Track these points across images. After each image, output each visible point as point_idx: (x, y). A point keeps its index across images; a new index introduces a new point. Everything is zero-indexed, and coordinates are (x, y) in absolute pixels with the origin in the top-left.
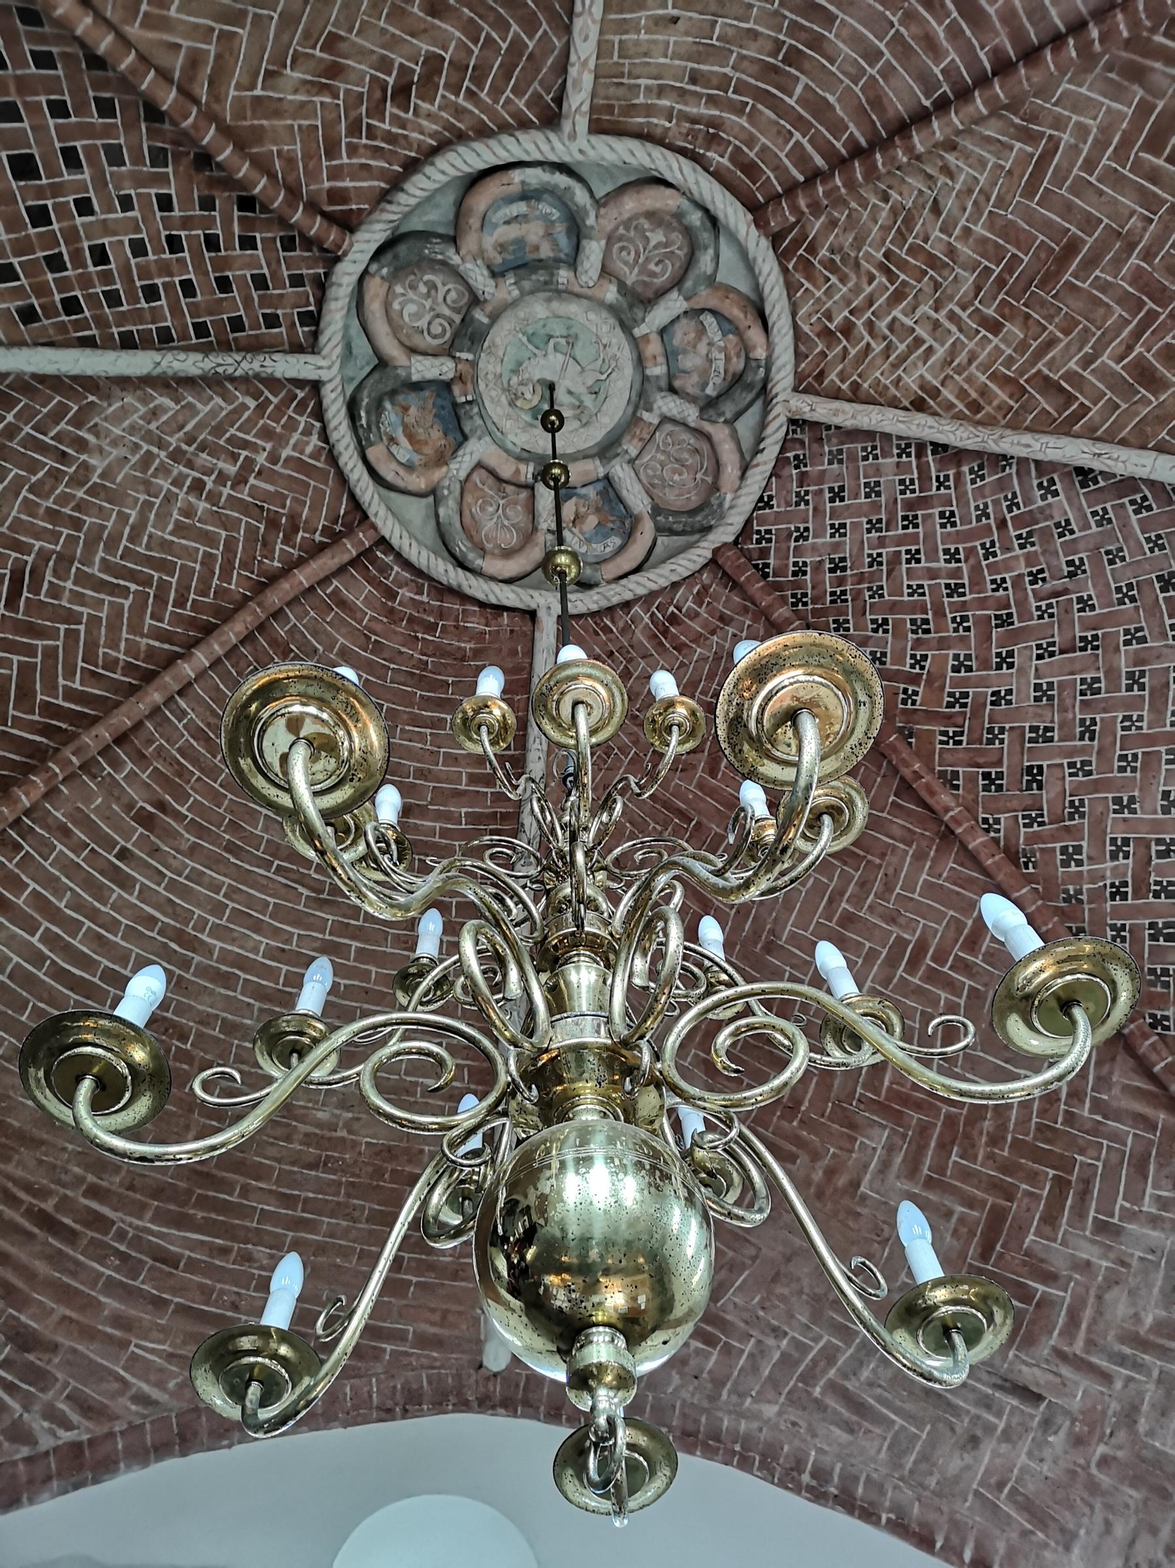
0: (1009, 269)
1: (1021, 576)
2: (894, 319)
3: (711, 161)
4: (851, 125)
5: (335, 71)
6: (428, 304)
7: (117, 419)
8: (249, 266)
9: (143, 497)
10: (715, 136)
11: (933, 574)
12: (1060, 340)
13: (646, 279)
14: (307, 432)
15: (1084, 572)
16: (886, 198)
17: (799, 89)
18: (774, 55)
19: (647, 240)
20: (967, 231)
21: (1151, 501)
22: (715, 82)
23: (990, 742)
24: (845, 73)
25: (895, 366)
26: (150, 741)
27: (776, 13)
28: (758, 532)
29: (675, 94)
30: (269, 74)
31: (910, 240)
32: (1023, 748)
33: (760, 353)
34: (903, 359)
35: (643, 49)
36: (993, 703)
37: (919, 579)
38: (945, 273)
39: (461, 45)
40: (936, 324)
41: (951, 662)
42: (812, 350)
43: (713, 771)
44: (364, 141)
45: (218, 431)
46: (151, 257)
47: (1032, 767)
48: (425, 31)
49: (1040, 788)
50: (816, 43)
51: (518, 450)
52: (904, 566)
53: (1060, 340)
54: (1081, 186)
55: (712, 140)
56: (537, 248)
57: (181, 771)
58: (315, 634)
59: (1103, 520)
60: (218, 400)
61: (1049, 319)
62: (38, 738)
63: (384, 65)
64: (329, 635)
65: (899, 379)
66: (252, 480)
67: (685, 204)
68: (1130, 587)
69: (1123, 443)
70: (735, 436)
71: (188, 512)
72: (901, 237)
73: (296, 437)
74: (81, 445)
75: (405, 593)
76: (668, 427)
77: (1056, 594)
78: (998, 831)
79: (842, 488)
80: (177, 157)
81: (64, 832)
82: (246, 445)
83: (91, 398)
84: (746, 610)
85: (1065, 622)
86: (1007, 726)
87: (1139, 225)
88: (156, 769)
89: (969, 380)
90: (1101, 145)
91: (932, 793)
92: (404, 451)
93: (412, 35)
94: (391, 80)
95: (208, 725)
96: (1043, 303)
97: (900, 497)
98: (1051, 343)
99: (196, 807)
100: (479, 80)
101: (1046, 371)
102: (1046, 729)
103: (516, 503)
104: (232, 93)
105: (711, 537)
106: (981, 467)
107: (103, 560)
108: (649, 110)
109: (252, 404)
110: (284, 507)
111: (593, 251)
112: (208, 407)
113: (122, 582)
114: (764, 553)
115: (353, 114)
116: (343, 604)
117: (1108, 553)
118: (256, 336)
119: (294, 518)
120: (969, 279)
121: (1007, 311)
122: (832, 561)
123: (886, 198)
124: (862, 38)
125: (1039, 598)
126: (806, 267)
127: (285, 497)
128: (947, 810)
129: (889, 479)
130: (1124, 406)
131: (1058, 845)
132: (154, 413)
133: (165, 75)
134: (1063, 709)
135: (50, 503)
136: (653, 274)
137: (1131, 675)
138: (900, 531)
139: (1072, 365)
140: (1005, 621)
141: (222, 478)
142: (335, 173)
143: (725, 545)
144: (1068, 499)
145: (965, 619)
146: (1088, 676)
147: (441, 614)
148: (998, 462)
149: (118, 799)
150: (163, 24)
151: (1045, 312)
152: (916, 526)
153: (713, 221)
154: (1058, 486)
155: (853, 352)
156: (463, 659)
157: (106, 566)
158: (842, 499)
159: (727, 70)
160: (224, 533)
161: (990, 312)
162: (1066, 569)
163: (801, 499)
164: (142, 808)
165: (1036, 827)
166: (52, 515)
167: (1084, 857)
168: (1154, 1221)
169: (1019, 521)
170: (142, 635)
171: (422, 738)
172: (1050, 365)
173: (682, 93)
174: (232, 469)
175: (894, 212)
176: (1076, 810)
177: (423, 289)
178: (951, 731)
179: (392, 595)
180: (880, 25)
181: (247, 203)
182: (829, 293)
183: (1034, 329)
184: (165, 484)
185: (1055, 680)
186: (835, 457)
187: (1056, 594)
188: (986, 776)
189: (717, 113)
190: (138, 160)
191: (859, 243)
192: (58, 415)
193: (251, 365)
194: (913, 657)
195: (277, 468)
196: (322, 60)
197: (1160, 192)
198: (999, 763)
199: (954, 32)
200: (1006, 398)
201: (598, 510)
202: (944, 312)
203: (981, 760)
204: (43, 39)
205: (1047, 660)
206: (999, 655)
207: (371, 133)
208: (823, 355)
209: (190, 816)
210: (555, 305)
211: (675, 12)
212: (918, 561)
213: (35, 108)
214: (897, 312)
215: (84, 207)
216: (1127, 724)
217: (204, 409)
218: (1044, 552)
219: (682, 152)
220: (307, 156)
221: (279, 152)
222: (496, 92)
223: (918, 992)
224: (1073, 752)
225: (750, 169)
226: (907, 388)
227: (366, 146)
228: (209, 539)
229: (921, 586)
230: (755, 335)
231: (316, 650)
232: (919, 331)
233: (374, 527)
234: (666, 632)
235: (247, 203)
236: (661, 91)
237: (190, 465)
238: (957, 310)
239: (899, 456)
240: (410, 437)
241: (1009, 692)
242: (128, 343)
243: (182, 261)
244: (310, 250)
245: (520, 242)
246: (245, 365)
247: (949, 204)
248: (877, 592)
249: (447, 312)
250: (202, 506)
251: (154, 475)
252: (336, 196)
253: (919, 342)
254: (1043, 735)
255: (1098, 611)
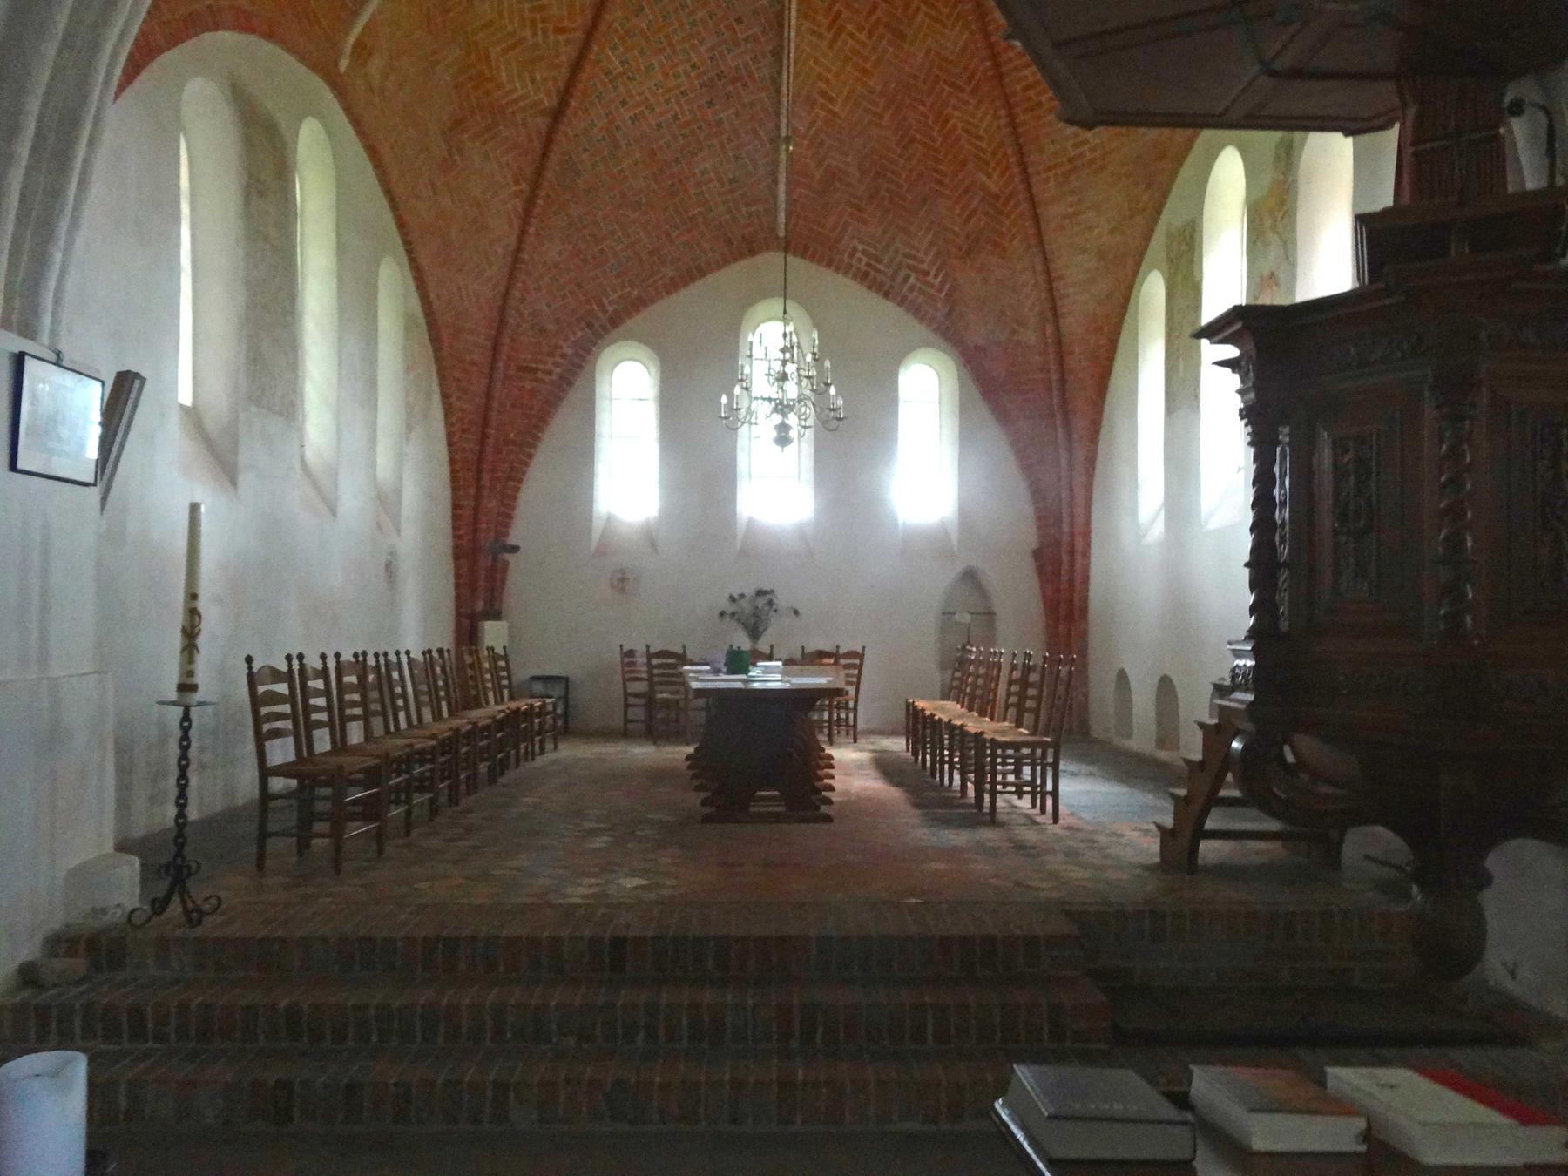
168: (501, 166)
223: (523, 20)
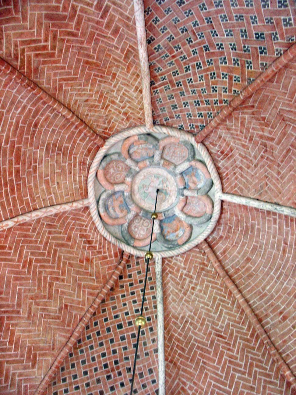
0: (97, 76)
1: (190, 46)
2: (120, 102)
3: (89, 162)
4: (71, 130)
5: (88, 260)
6: (140, 228)
7: (175, 309)
8: (136, 276)
9: (197, 302)
10: (83, 163)
11: (195, 74)
12: (113, 57)
13: (124, 169)
14: (177, 260)
15: (184, 27)
16: (87, 115)
17: (67, 145)
18: (60, 154)
19: (113, 173)
20: (90, 90)
21: (154, 18)
22: (70, 167)
23: (249, 51)
24: (60, 136)
25: (132, 99)
26: (262, 312)
27: (51, 157)
28: (191, 128)
29: (75, 177)
30: (90, 276)
31: (97, 104)
32: (250, 40)
33: (136, 138)
34: (130, 98)
35: (66, 189)
36: (235, 50)
37: (197, 78)
38: (103, 92)
39: (76, 230)
40: (118, 90)
41: (223, 65)
42: (133, 122)
43: (272, 139)
44: (102, 249)
45: (178, 284)
46: (136, 299)
47: (256, 37)
48: (75, 240)
49: (263, 34)
50: (54, 145)
51: (177, 199)
52: (194, 83)
53: (113, 57)
54: (70, 67)
55: (84, 163)
56: (121, 202)
57: (272, 305)
58: (233, 261)
59: (165, 29)
60: (169, 284)
61: (107, 61)
62: (259, 342)
63: (84, 248)
64: (234, 257)
65: (135, 97)
66: (191, 274)
67: (101, 168)
68: (186, 13)
69: (136, 34)
70: (163, 139)
71: (201, 291)
72: (97, 106)
73: (178, 263)
74: (183, 318)
75: (221, 233)
76: (164, 156)
77: (194, 34)
78: (281, 50)
79: (172, 106)
80: (112, 295)
81: (285, 342)
82: (181, 276)
83: (170, 316)
84: (215, 132)
85: (203, 28)
86: (243, 45)
87: (74, 48)
88: (271, 312)
89: (131, 79)
90: (57, 68)
91: (267, 76)
92: (180, 233)
93: (76, 242)
94: (87, 245)
95: (259, 295)
96: (104, 64)
97: (171, 89)
98: (114, 59)
99: (283, 303)
100: (83, 225)
101: (123, 59)
102: (242, 31)
103: (192, 200)
104: (96, 284)
105: (194, 144)
106: (156, 70)
107: (214, 313)
108: (80, 183)
109: (170, 275)
110: (198, 266)
111: (117, 188)
112: (171, 287)
113: (219, 310)
114: (197, 127)
115: (96, 253)
116: (224, 252)
117: (176, 23)
118: (152, 274)
119: (200, 264)
120: (103, 85)
121: (109, 73)
122: (196, 105)
123: (87, 115)
124: (50, 135)
125: (197, 39)
126: (111, 129)
127: (195, 266)
128: (273, 71)
129: (166, 94)
130: (126, 36)
131: (284, 28)
132: (174, 300)
133: (94, 301)
134: (233, 26)
135: (199, 325)
136: (122, 168)
137: (217, 6)
138: (183, 86)
139: (119, 52)
140: (207, 48)
141: (191, 282)
142: (111, 256)
143: (195, 139)
144: (160, 41)
145: (208, 62)
146: (220, 19)
147: (226, 224)
148: (152, 66)
149: (277, 325)
150: (83, 301)
151: (106, 63)
152: (180, 82)
153: (105, 157)
154: (156, 46)
155: (131, 111)
156: (238, 220)
157: (215, 313)
158: (176, 105)
159: (67, 165)
160: (205, 283)
161: (110, 77)
162: (185, 33)
163: (178, 117)
164: (281, 318)
165: (278, 36)
166: (202, 325)
167: (287, 18)
169: (171, 52)
170: (233, 308)
171: (263, 235)
172: (121, 58)
173: (74, 175)
174: (188, 279)
175: (90, 111)
176: (270, 21)
177: (136, 229)
178: (247, 65)
179: (221, 237)
180: (47, 131)
181: (121, 277)
182: (117, 121)
183: (111, 64)
184: (193, 297)
185: (224, 30)
186: (163, 110)
187: (194, 34)
188: (261, 53)
189: (77, 164)
190: (115, 303)
191: (101, 117)
192: (175, 324)
193: (158, 276)
194: (223, 78)
195: (187, 268)
196: (86, 263)
197: (64, 47)
198: (256, 48)
199: (42, 115)
200: (133, 68)
201: (191, 176)
202: (114, 89)
203: (256, 55)
204: (92, 325)
205: (217, 33)
206: (219, 49)
207: (100, 248)
208: (134, 119)
209: (285, 305)
210: (135, 193)
211: (56, 184)
212: (191, 79)
213: (107, 325)
214: (117, 102)
215: (127, 314)
216: (235, 5)
217: (172, 288)
218: (180, 41)
219: (88, 171)
220: (107, 264)
221: (108, 271)
222: (84, 221)
224: (248, 23)
225: (89, 151)
226: (138, 95)
227: (103, 249)
228: (207, 287)
229: (199, 77)
230: (132, 140)
231: (238, 261)
232: (121, 94)
233: (201, 243)
234: (227, 155)
235: (121, 277)
236: (75, 181)
237: (187, 291)
238: (112, 86)
239: (158, 93)
240: (176, 231)
241: (231, 45)
242: (155, 307)
243: (137, 292)
244: (130, 261)
245: (119, 207)
246: (159, 279)
247: (85, 98)
248: (204, 91)
249: (142, 222)
250: (198, 287)
251: (191, 299)
252: (116, 255)
253: (124, 94)
254: (244, 33)
255: (197, 20)
